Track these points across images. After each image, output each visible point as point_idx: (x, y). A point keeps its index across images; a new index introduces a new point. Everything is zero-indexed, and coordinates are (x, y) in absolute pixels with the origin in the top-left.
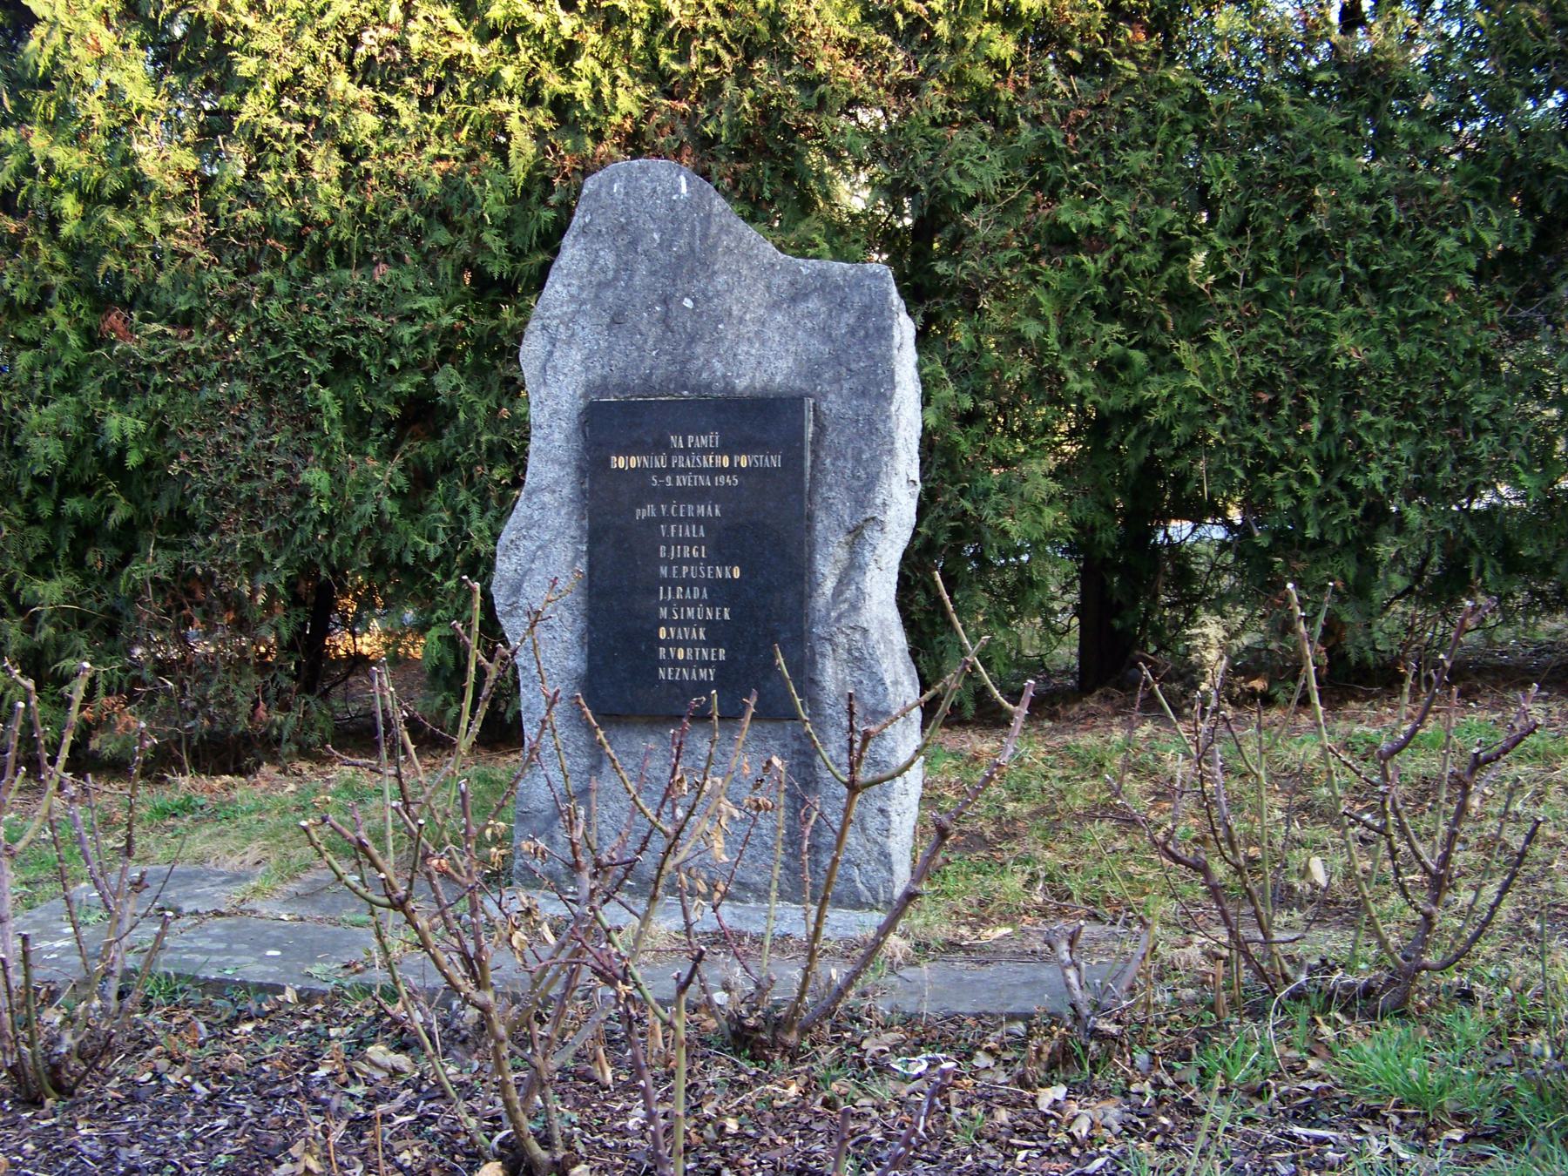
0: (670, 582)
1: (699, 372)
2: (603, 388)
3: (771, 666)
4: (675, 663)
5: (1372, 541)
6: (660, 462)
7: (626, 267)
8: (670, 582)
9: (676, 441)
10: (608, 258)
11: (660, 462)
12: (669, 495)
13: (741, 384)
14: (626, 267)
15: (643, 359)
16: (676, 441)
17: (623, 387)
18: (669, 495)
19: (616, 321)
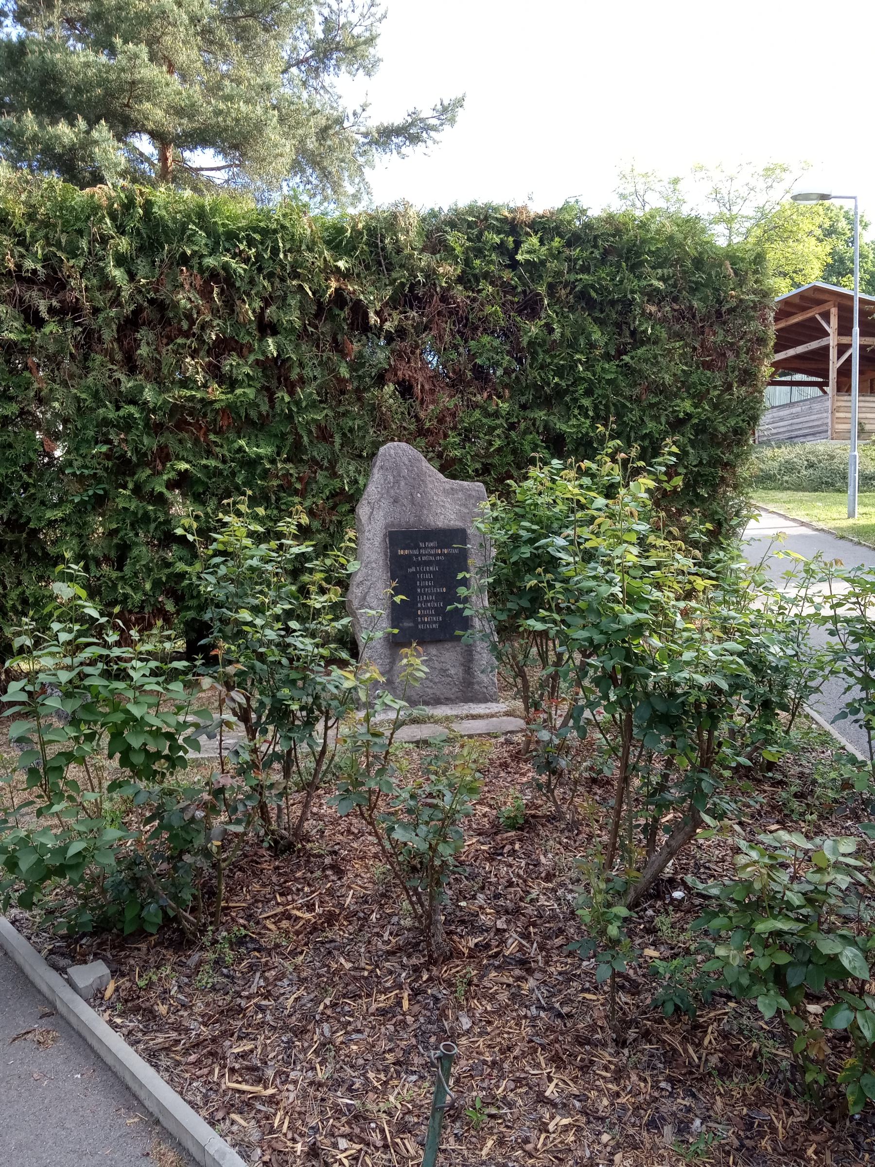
0: (421, 594)
1: (174, 219)
2: (393, 525)
3: (442, 586)
4: (424, 623)
5: (146, 403)
6: (416, 552)
7: (397, 482)
8: (421, 594)
9: (421, 545)
10: (390, 478)
11: (416, 552)
12: (419, 564)
13: (440, 524)
14: (397, 482)
15: (407, 518)
16: (421, 545)
17: (400, 525)
18: (419, 564)
19: (396, 501)
